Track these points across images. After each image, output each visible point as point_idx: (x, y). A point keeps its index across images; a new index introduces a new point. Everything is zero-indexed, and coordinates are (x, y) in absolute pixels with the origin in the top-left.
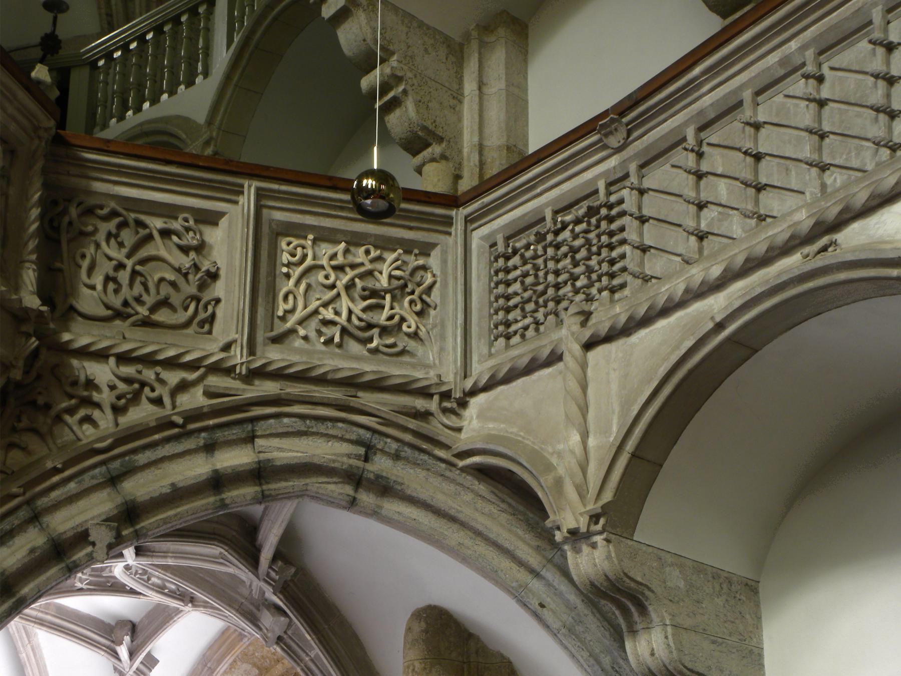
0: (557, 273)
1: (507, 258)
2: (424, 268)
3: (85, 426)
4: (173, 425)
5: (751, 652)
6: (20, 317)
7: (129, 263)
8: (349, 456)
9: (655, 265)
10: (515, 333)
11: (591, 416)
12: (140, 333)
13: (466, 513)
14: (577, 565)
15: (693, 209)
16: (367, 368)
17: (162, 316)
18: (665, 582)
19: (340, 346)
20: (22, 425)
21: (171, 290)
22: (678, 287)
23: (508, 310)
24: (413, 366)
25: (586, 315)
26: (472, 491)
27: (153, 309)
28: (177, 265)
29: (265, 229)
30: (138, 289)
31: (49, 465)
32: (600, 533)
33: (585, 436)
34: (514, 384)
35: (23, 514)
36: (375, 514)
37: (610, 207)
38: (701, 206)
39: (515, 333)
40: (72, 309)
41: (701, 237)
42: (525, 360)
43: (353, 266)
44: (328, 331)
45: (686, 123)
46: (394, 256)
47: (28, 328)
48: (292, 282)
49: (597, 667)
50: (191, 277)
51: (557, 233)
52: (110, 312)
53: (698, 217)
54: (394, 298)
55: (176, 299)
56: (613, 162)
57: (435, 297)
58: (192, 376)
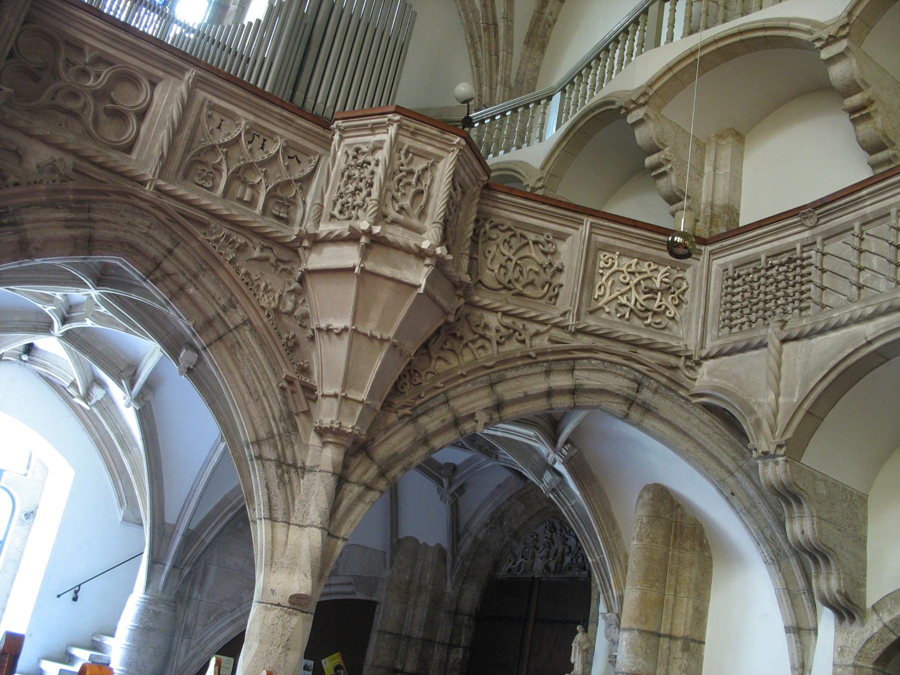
0: (766, 294)
1: (734, 280)
2: (682, 278)
3: (480, 351)
4: (530, 357)
5: (860, 538)
6: (457, 285)
7: (514, 259)
8: (628, 388)
9: (829, 299)
10: (736, 325)
11: (782, 384)
12: (515, 300)
13: (694, 432)
14: (764, 473)
15: (855, 270)
16: (644, 336)
17: (528, 291)
18: (815, 490)
19: (628, 320)
20: (446, 347)
21: (535, 277)
22: (843, 315)
23: (732, 311)
24: (671, 337)
25: (785, 322)
26: (699, 418)
27: (524, 287)
28: (540, 262)
29: (593, 246)
30: (517, 274)
31: (459, 372)
32: (782, 456)
33: (778, 395)
34: (733, 357)
35: (442, 398)
36: (638, 425)
37: (803, 260)
38: (861, 269)
39: (736, 325)
40: (480, 281)
41: (860, 287)
42: (743, 344)
43: (640, 273)
44: (622, 310)
45: (855, 220)
46: (665, 269)
47: (460, 292)
48: (604, 278)
49: (761, 536)
50: (547, 270)
51: (767, 270)
52: (500, 286)
53: (859, 275)
54: (662, 294)
55: (538, 282)
56: (807, 234)
57: (687, 297)
58: (543, 328)
